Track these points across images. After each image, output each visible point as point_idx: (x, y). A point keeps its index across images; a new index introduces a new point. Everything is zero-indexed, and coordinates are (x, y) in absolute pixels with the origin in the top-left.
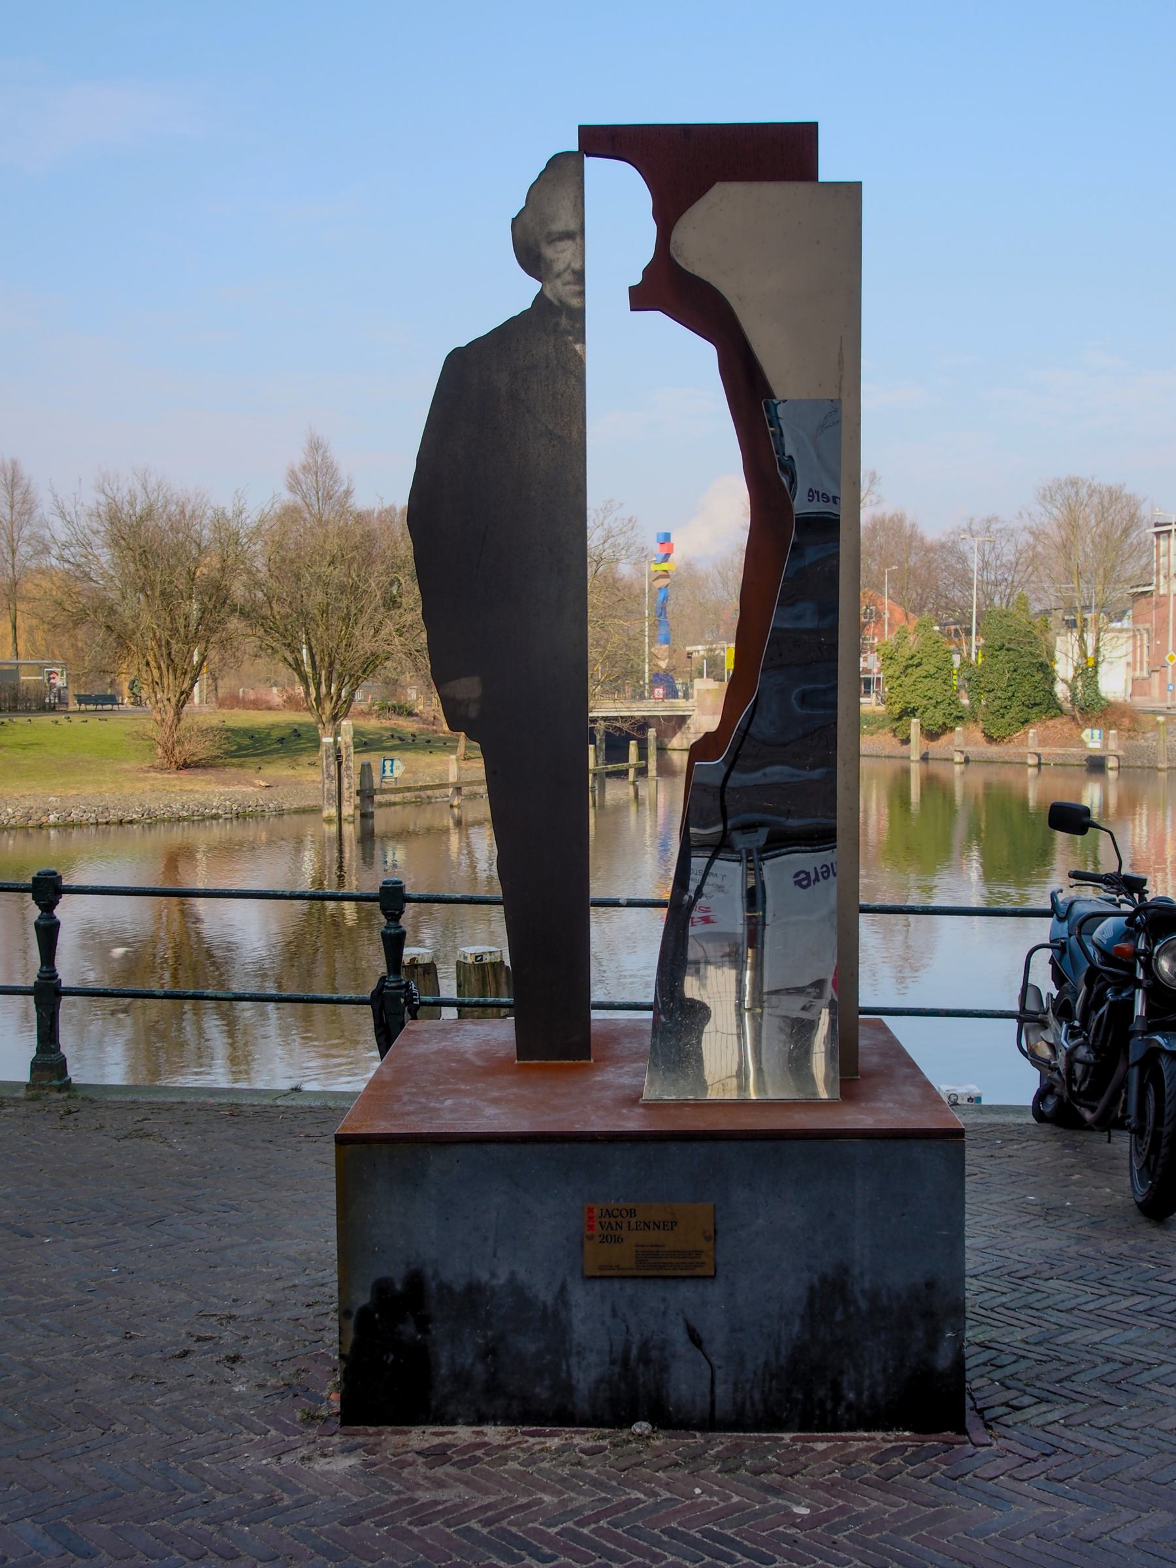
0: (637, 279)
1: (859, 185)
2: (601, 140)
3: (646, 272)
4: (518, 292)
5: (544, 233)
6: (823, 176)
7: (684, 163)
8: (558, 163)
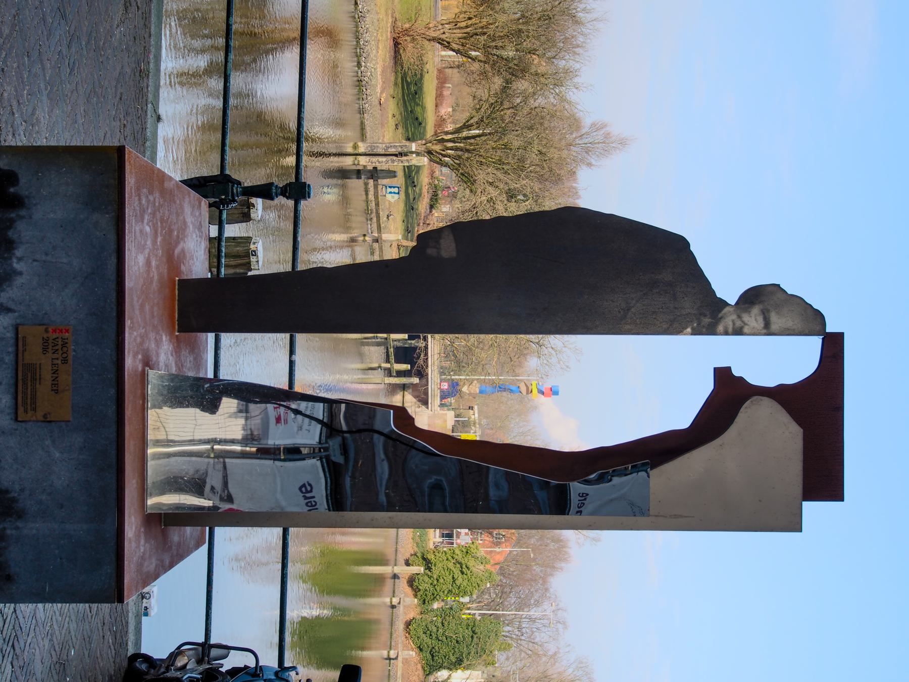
0: (736, 373)
1: (801, 531)
2: (833, 346)
3: (741, 379)
4: (728, 290)
5: (767, 306)
6: (806, 505)
7: (817, 405)
8: (819, 317)
